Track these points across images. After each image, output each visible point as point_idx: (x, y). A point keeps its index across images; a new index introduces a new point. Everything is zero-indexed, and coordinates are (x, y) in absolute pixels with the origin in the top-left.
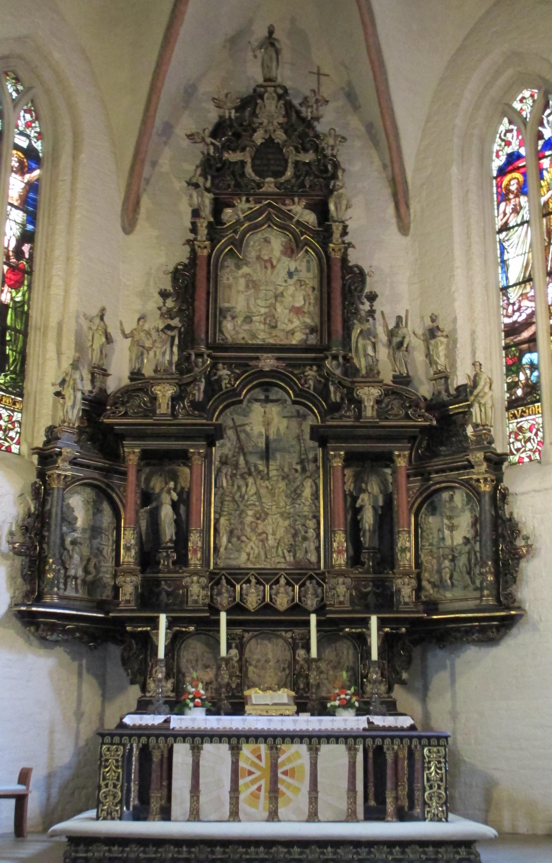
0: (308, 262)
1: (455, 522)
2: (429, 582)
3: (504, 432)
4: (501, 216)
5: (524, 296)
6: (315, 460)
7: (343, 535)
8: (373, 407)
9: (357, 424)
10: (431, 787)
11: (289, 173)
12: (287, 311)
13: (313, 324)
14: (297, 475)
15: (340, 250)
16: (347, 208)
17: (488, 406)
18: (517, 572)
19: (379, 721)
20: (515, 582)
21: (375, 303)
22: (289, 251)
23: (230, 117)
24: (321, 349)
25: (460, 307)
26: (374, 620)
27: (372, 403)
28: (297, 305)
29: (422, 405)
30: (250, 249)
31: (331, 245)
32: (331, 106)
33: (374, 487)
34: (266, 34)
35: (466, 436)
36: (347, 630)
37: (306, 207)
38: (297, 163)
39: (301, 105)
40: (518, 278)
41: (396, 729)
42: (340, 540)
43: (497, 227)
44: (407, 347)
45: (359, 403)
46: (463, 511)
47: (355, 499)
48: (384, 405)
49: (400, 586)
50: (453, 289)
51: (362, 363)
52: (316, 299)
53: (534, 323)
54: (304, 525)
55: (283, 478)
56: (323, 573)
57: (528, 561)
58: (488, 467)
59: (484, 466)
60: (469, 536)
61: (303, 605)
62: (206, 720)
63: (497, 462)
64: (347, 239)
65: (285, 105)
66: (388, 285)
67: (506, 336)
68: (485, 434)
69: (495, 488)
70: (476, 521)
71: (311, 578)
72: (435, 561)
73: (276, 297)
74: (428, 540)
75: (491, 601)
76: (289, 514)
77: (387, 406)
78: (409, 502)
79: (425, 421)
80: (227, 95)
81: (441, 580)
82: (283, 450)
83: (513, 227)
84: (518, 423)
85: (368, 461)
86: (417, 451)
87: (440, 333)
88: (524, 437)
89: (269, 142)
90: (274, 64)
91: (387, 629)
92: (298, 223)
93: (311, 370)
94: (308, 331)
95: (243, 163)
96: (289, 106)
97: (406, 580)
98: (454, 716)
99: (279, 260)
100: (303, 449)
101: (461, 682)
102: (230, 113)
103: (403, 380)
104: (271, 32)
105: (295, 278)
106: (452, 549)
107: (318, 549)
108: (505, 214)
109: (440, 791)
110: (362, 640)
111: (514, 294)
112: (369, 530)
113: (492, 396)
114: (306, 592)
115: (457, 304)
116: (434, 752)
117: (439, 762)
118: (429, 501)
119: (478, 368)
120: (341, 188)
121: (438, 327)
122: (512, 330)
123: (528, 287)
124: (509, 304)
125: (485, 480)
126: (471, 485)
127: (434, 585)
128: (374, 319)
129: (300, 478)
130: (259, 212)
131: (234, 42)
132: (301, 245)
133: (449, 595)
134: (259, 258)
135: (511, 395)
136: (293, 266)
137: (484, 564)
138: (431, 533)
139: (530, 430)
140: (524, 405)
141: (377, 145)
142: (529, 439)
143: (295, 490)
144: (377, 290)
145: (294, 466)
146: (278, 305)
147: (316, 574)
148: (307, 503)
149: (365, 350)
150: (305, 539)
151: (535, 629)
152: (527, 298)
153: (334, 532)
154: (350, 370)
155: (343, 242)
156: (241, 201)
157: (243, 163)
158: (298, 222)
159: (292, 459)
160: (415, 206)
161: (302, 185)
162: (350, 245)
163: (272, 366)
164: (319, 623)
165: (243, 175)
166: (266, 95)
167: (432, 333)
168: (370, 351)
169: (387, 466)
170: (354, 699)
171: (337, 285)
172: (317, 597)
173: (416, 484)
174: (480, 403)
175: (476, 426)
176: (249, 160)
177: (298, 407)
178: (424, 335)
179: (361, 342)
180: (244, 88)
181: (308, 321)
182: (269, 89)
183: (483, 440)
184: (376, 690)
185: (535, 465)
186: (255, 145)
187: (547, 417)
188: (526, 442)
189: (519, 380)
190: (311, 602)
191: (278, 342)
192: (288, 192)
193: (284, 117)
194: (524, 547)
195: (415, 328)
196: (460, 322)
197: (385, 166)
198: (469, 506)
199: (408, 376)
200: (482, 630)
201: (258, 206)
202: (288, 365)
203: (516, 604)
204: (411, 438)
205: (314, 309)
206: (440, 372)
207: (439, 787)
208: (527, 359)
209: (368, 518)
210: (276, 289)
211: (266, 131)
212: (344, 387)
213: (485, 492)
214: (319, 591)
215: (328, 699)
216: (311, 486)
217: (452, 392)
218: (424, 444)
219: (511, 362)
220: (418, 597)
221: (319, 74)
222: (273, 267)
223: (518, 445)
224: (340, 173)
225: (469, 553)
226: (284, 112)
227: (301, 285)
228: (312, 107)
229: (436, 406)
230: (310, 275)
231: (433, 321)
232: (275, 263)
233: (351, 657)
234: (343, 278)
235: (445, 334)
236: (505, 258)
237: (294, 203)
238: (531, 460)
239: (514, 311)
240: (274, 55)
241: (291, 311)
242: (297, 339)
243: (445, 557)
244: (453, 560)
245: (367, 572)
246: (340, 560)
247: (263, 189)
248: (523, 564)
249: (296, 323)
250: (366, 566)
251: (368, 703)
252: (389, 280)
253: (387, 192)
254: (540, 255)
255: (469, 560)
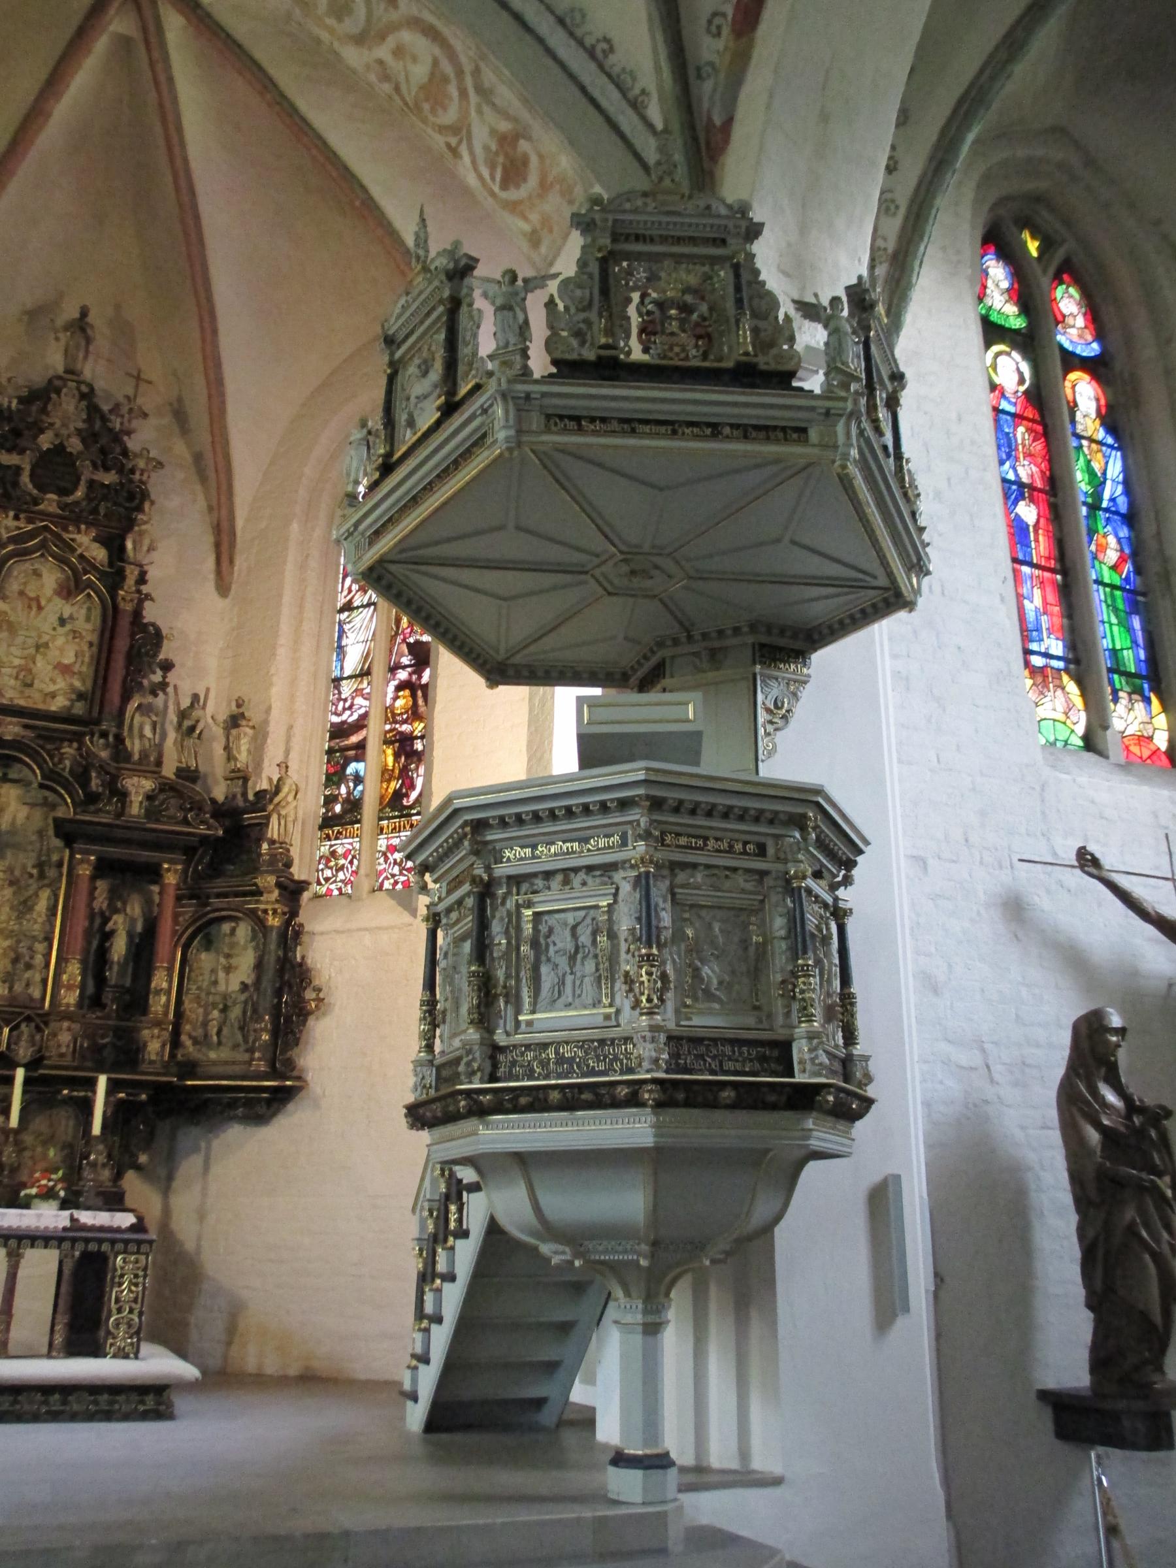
0: (89, 609)
1: (233, 961)
2: (190, 1037)
3: (312, 854)
4: (345, 593)
5: (358, 692)
6: (60, 864)
7: (78, 965)
8: (141, 803)
9: (117, 822)
10: (119, 1311)
11: (79, 494)
12: (50, 667)
13: (82, 689)
14: (31, 881)
15: (132, 600)
16: (148, 551)
17: (290, 819)
18: (301, 1032)
19: (87, 1217)
20: (297, 1045)
21: (169, 675)
22: (65, 591)
23: (9, 407)
24: (89, 722)
25: (277, 693)
26: (102, 1081)
27: (140, 798)
28: (66, 662)
29: (208, 807)
30: (12, 580)
31: (121, 592)
32: (153, 421)
33: (135, 908)
34: (77, 315)
35: (260, 855)
36: (66, 1092)
37: (95, 540)
38: (91, 484)
39: (111, 411)
40: (355, 669)
41: (110, 1229)
42: (74, 970)
43: (339, 605)
44: (200, 733)
45: (123, 795)
46: (245, 948)
47: (106, 920)
48: (157, 803)
49: (148, 1038)
50: (273, 671)
51: (135, 746)
52: (92, 657)
53: (365, 726)
54: (30, 948)
55: (11, 883)
56: (48, 1014)
57: (317, 1019)
58: (280, 895)
59: (276, 893)
60: (249, 981)
61: (12, 1055)
62: (57, 1216)
63: (292, 891)
64: (144, 589)
65: (88, 407)
66: (191, 655)
67: (332, 738)
68: (281, 853)
69: (288, 923)
70: (259, 966)
71: (28, 1019)
72: (201, 1010)
73: (37, 647)
74: (195, 982)
75: (263, 1067)
76: (12, 931)
77: (162, 804)
78: (175, 932)
79: (208, 829)
80: (9, 380)
81: (206, 1036)
82: (17, 847)
83: (358, 608)
84: (331, 846)
85: (127, 872)
86: (196, 866)
87: (244, 723)
88: (336, 865)
89: (59, 449)
90: (81, 355)
91: (122, 1095)
92: (82, 557)
93: (70, 746)
94: (74, 697)
95: (18, 470)
96: (93, 410)
97: (156, 1031)
98: (202, 1216)
99: (49, 600)
100: (45, 848)
101: (216, 1169)
102: (10, 402)
103: (188, 775)
104: (84, 313)
105: (68, 627)
106: (225, 997)
107: (44, 982)
108: (350, 591)
109: (131, 1316)
110: (86, 1107)
111: (347, 688)
112: (119, 962)
113: (296, 807)
114: (19, 1037)
115: (274, 690)
116: (130, 1262)
117: (136, 1276)
118: (203, 932)
119: (284, 770)
120: (146, 523)
121: (243, 715)
122: (339, 731)
123: (365, 682)
124: (340, 699)
125: (275, 911)
126: (258, 918)
127: (196, 1042)
128: (166, 694)
129: (35, 887)
130: (31, 535)
131: (35, 316)
132: (82, 586)
133: (213, 1055)
134: (22, 593)
135: (327, 811)
136: (67, 611)
137: (260, 1019)
138: (202, 974)
139: (345, 856)
140: (342, 825)
141: (203, 479)
142: (342, 868)
143: (25, 902)
144: (176, 660)
145: (29, 869)
146: (39, 658)
147: (39, 1015)
148: (40, 920)
149: (141, 729)
150: (29, 966)
151: (317, 1105)
152: (362, 696)
153: (67, 961)
154: (119, 751)
155: (139, 592)
156: (7, 516)
157: (18, 470)
158: (81, 556)
159: (28, 861)
160: (240, 563)
161: (95, 511)
162: (148, 597)
163: (17, 735)
164: (27, 1082)
165: (16, 484)
166: (64, 390)
167: (234, 721)
168: (148, 731)
169: (155, 882)
170: (59, 1186)
171: (122, 644)
172: (33, 1045)
173: (189, 910)
174: (279, 815)
175: (272, 842)
176: (27, 468)
177: (47, 793)
178: (225, 722)
179: (138, 719)
180: (37, 377)
181: (77, 684)
182: (70, 383)
183: (278, 861)
184: (98, 1175)
185: (344, 899)
186: (39, 449)
187: (364, 842)
188: (337, 871)
189: (339, 794)
190: (24, 1052)
191: (31, 705)
192: (73, 516)
193: (84, 421)
194: (314, 1000)
195: (215, 710)
196: (275, 713)
197: (210, 509)
198: (253, 944)
199: (197, 770)
200: (249, 1103)
201: (30, 527)
202: (39, 737)
203: (295, 1073)
204: (189, 850)
205: (86, 669)
206: (239, 770)
207: (131, 1311)
208: (351, 769)
209: (119, 947)
210: (40, 637)
211: (57, 435)
212: (107, 773)
213: (272, 927)
214: (38, 1037)
215: (24, 1186)
216: (49, 899)
217: (251, 797)
218: (207, 860)
219: (332, 770)
220: (172, 1055)
221: (138, 378)
222: (40, 608)
223: (328, 873)
224: (147, 505)
225: (246, 1002)
226: (85, 417)
227: (74, 638)
228: (122, 416)
229: (227, 813)
230: (89, 626)
231: (239, 706)
232: (43, 603)
233: (70, 1131)
234: (132, 635)
235: (251, 724)
236: (344, 643)
237: (79, 532)
238: (341, 894)
239: (344, 709)
240: (83, 343)
241: (55, 668)
242: (58, 704)
243: (214, 1005)
244: (225, 1010)
245: (108, 1017)
246: (70, 998)
247: (41, 507)
248: (311, 1022)
249: (61, 684)
250: (107, 1010)
251: (78, 1194)
252: (194, 648)
253: (209, 539)
254: (383, 643)
255: (244, 1012)
